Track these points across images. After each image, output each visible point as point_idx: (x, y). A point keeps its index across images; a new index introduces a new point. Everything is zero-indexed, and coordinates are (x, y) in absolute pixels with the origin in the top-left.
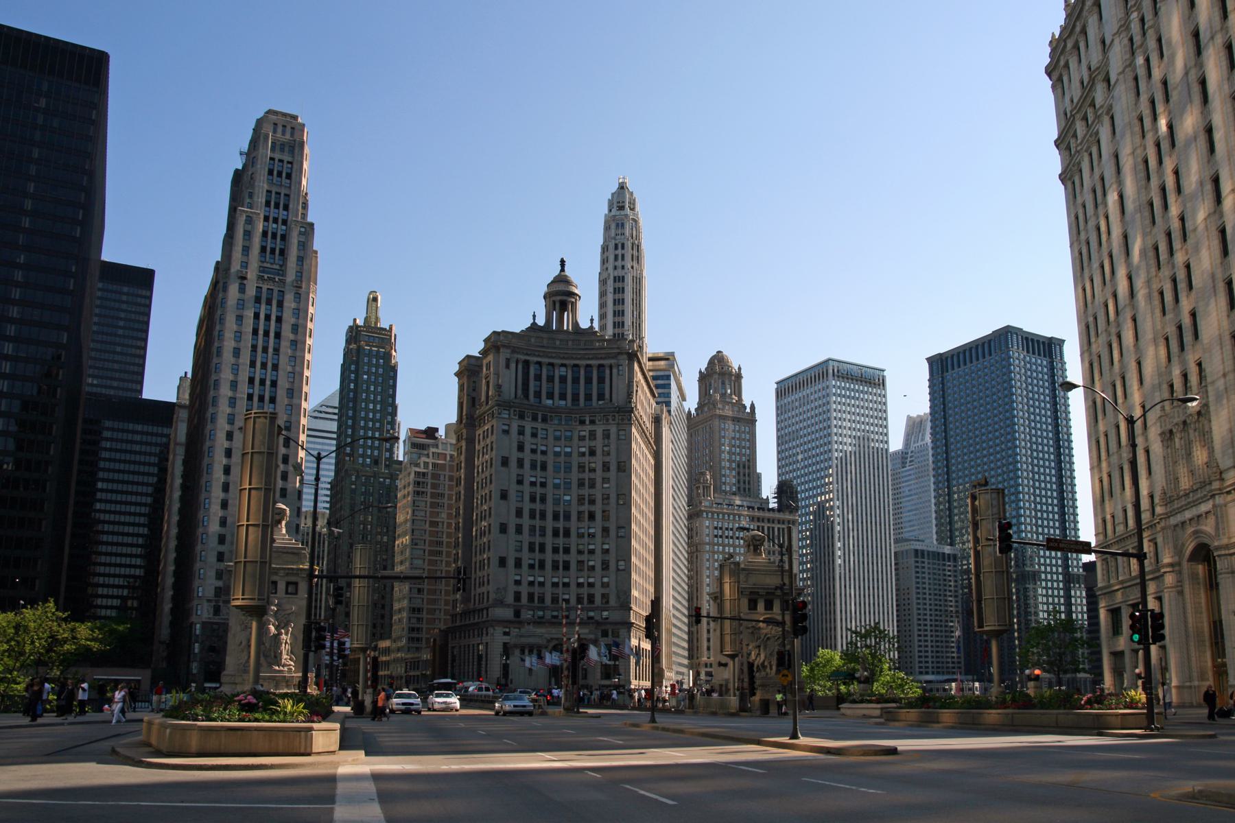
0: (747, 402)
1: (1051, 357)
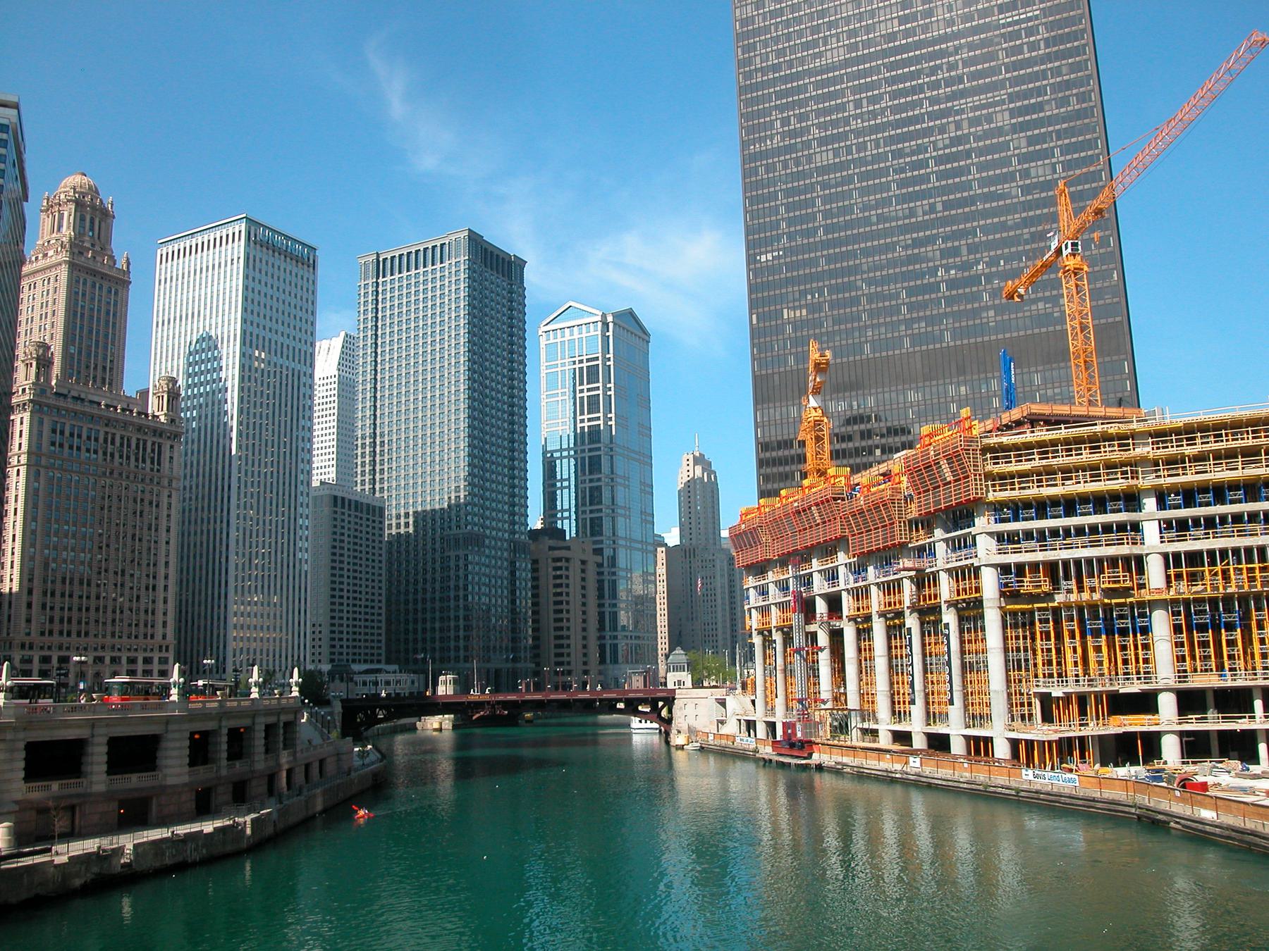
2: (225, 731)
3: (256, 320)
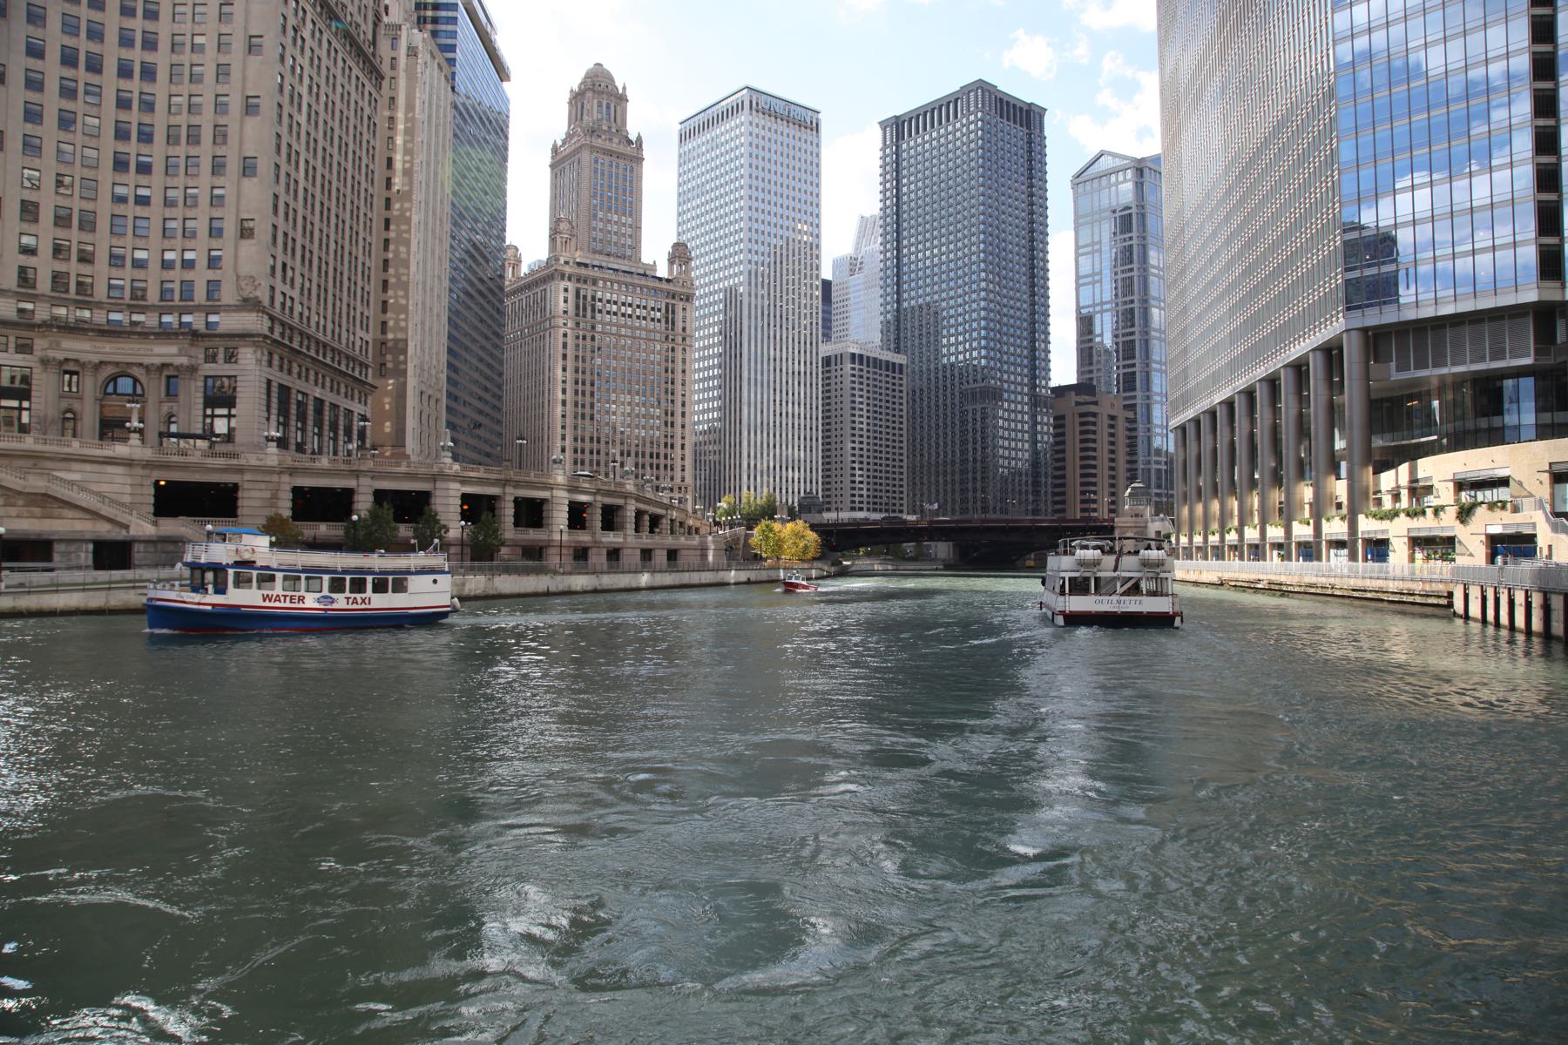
0: (633, 137)
1: (1029, 127)
2: (599, 505)
3: (761, 185)
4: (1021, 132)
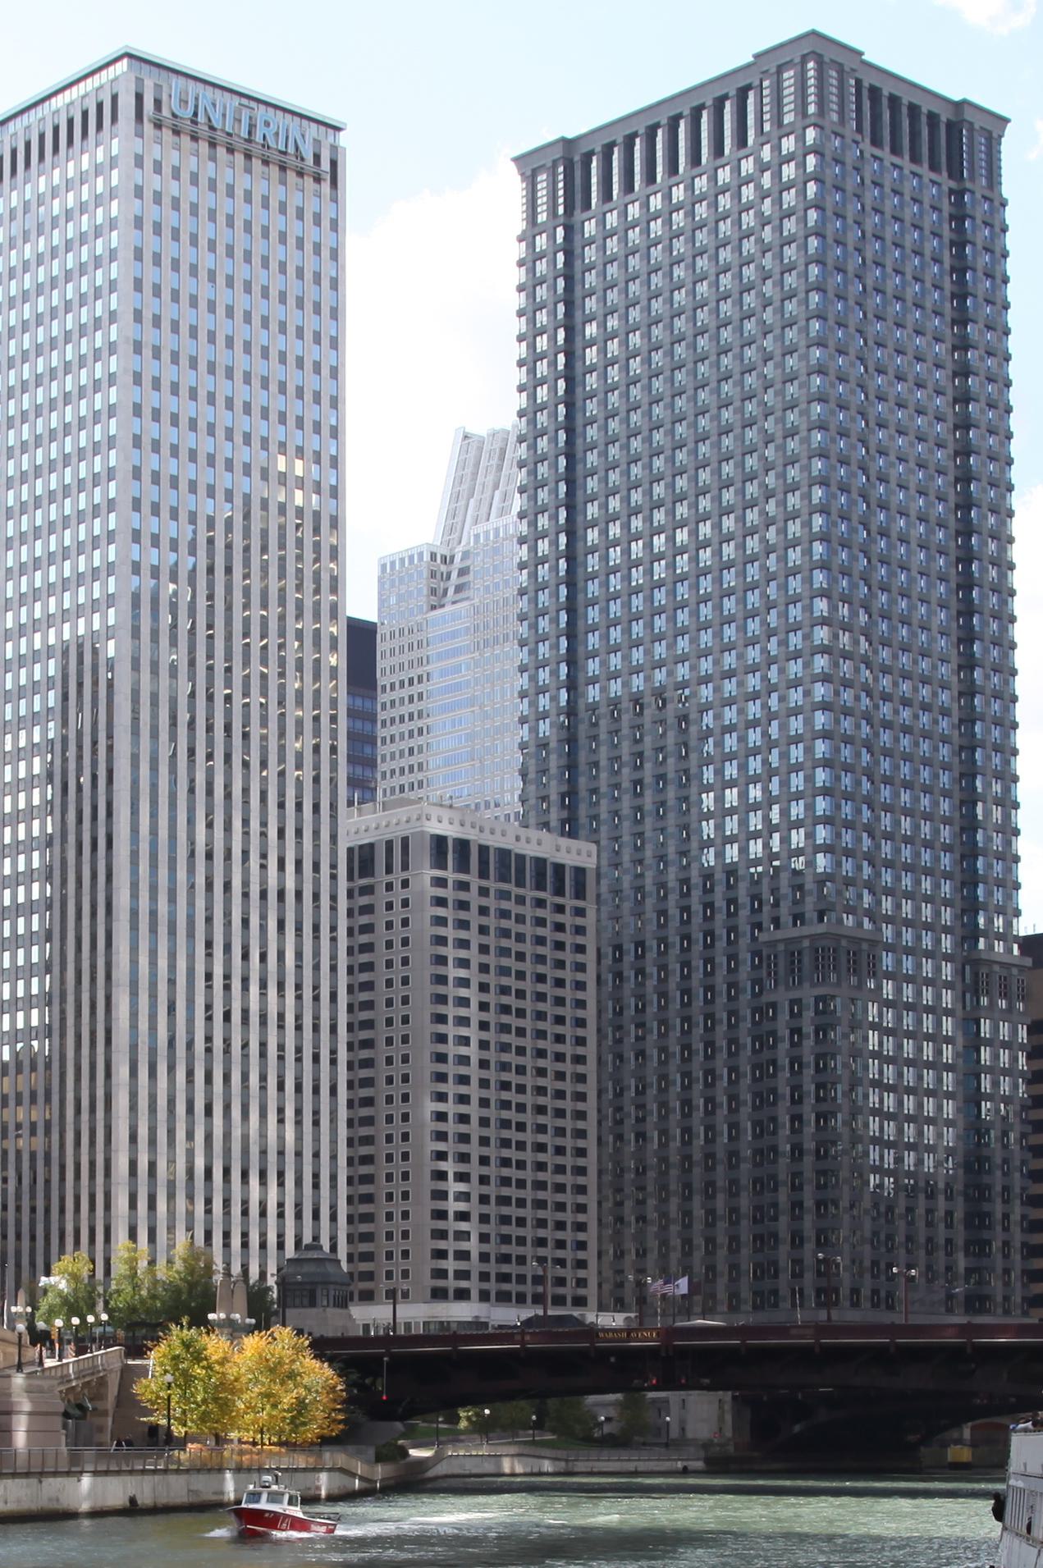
1: (955, 172)
4: (935, 185)
